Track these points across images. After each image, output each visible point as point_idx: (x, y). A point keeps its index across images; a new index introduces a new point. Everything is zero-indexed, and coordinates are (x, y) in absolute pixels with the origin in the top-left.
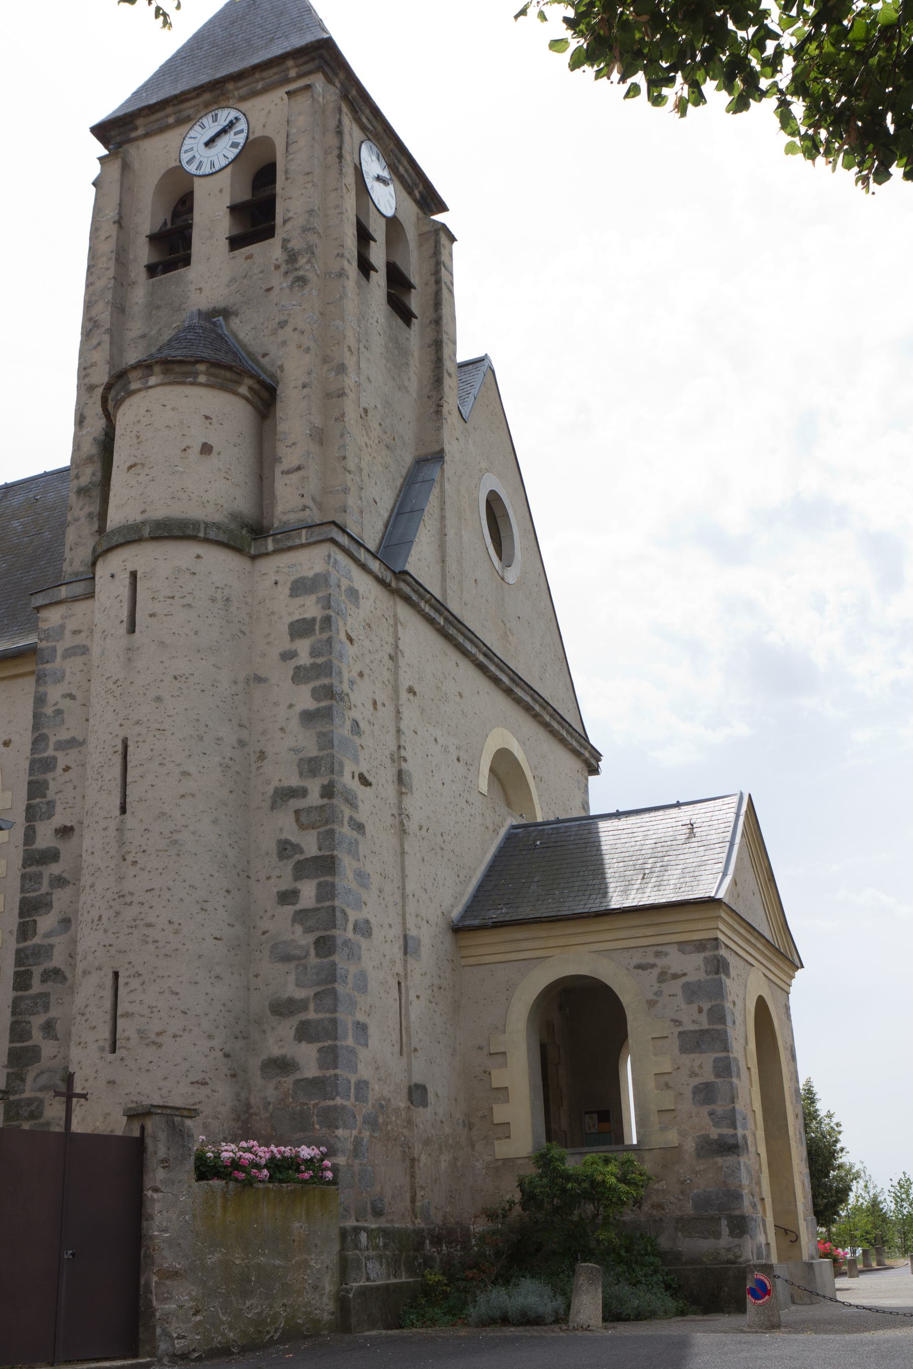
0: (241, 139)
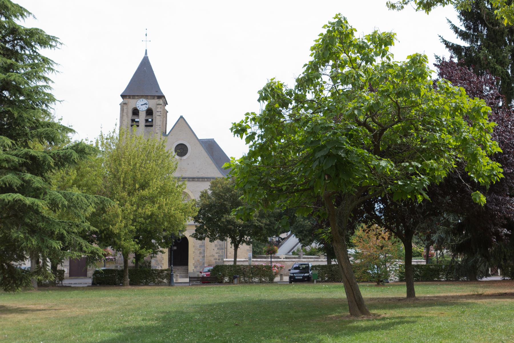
0: (147, 106)
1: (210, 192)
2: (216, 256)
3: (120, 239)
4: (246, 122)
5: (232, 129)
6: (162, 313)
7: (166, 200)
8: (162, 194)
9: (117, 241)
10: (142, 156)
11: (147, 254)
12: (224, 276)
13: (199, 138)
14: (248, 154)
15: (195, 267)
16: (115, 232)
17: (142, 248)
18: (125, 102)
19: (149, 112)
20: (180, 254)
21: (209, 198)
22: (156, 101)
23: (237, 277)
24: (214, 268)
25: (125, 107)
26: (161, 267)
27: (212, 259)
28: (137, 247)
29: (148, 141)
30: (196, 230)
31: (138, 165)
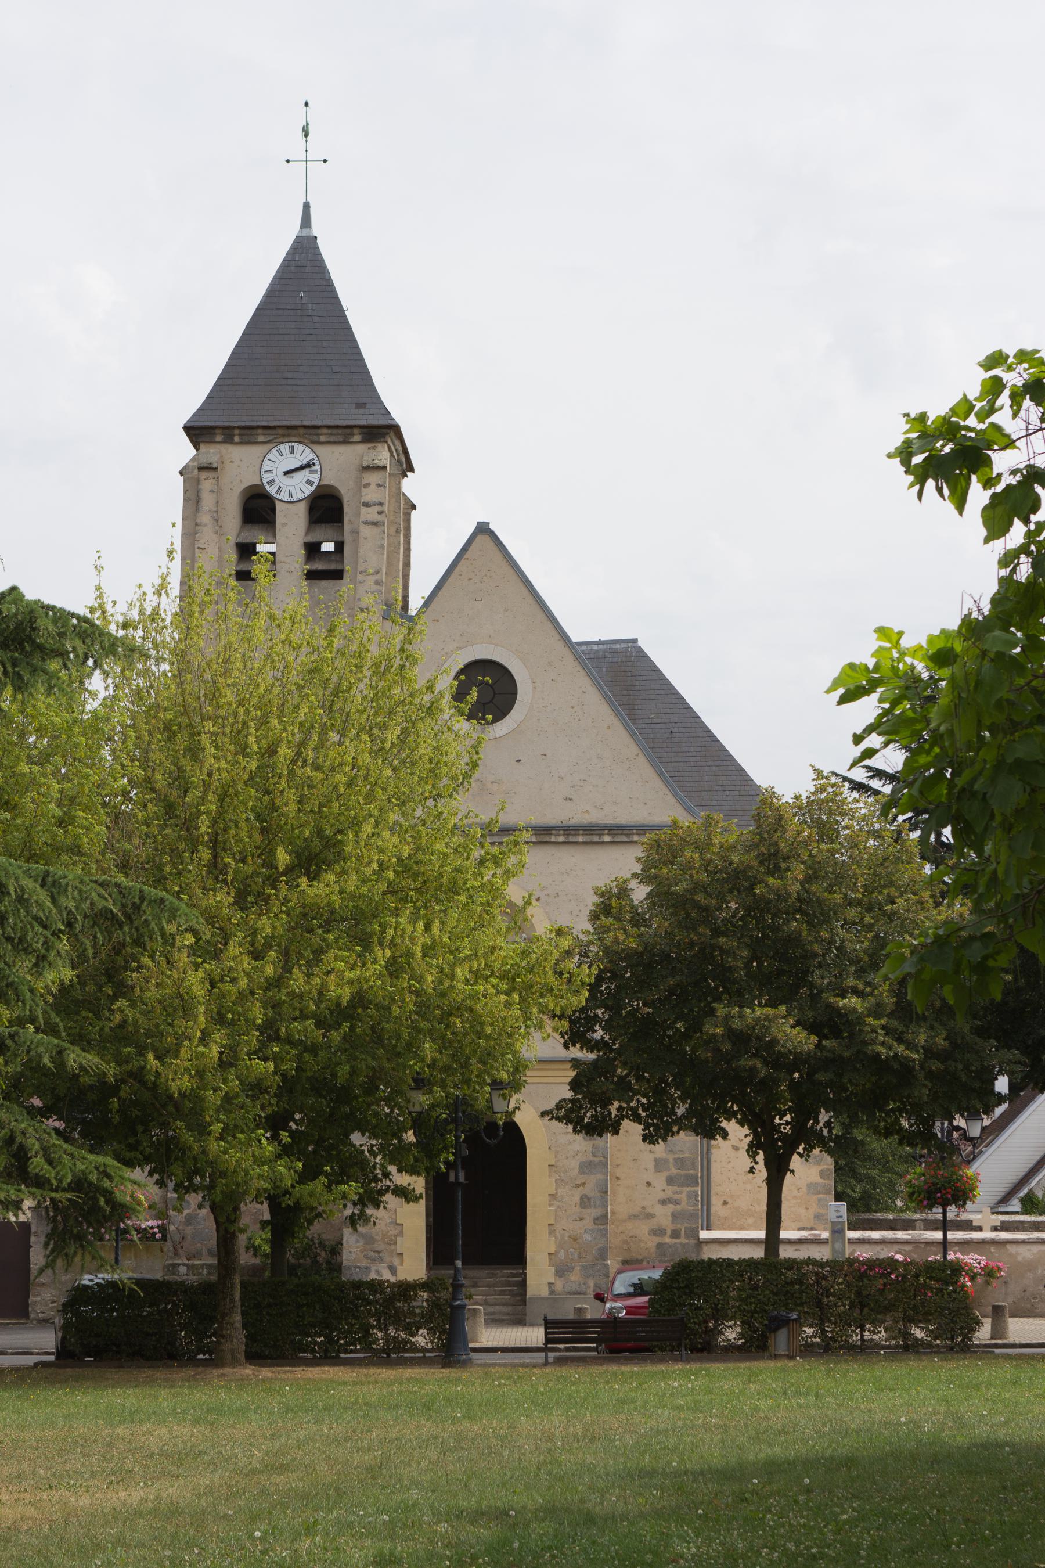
0: (315, 478)
1: (640, 893)
2: (663, 1216)
3: (202, 1130)
4: (992, 410)
5: (905, 453)
6: (478, 1516)
7: (428, 928)
8: (405, 900)
9: (188, 1138)
10: (304, 709)
11: (332, 1203)
12: (720, 1314)
13: (575, 638)
14: (995, 601)
15: (560, 1273)
16: (174, 1088)
17: (307, 1176)
18: (204, 461)
19: (326, 508)
20: (482, 1206)
21: (638, 920)
22: (355, 453)
23: (786, 1322)
24: (666, 1274)
25: (207, 485)
26: (393, 1270)
27: (642, 1230)
28: (285, 1171)
29: (331, 630)
30: (574, 1085)
31: (284, 752)
